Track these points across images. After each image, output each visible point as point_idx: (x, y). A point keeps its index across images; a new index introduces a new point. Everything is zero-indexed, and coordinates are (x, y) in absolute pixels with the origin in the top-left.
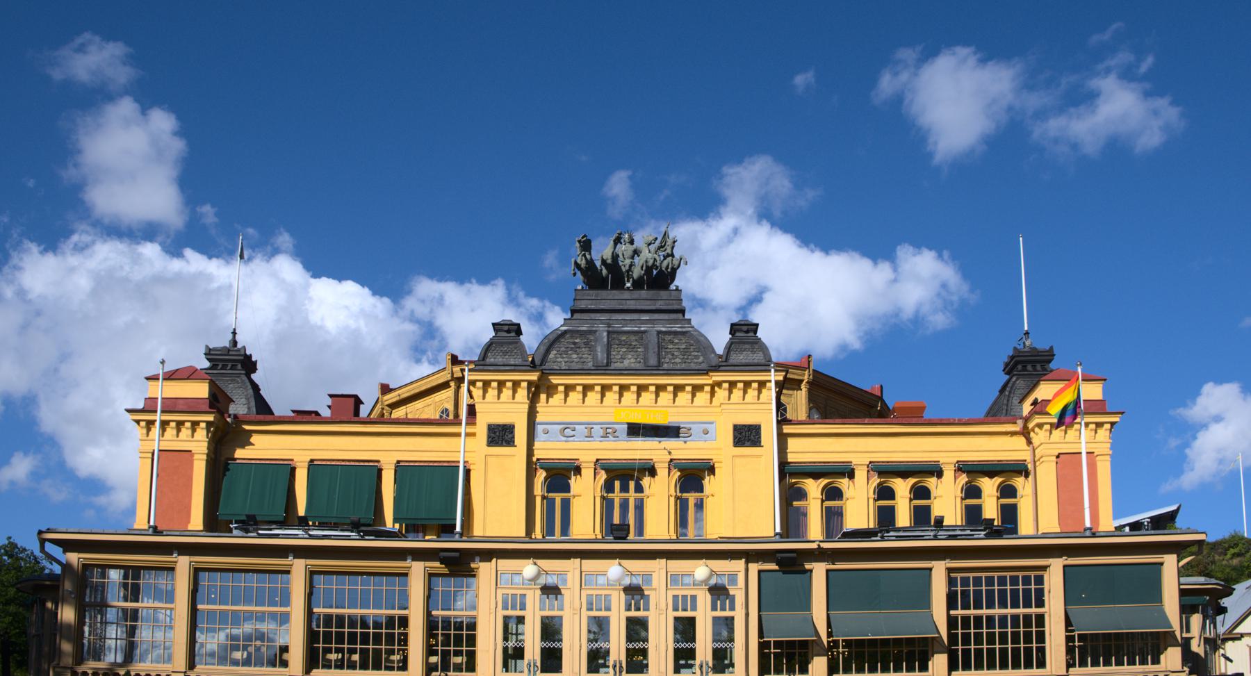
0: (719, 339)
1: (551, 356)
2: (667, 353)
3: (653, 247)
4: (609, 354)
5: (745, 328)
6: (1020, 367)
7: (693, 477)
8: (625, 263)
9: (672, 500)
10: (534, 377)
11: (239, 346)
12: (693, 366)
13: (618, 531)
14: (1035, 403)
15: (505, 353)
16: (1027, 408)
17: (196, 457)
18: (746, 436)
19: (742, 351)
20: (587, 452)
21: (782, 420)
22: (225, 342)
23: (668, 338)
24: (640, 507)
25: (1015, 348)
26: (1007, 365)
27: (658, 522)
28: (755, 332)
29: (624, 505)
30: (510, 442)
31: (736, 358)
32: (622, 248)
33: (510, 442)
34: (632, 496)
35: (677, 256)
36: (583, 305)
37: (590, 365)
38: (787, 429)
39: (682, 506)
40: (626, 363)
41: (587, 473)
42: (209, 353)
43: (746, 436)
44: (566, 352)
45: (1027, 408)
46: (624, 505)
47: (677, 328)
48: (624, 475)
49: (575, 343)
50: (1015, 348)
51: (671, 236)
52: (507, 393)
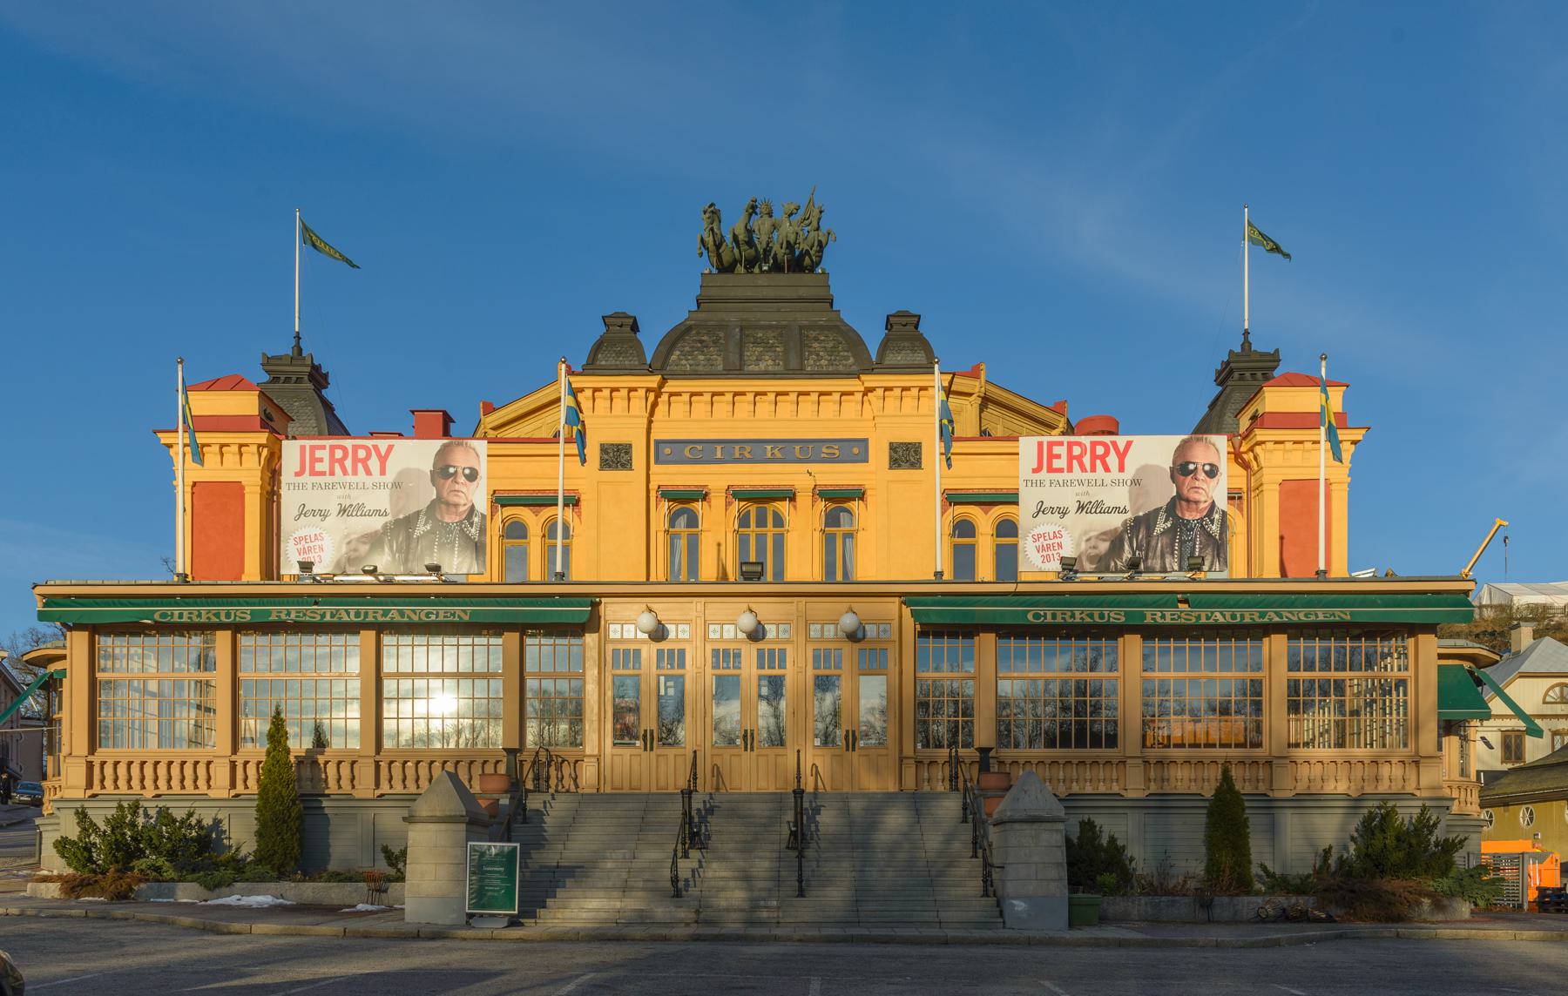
0: (873, 337)
1: (673, 357)
2: (811, 353)
3: (797, 218)
4: (741, 355)
5: (904, 320)
6: (1236, 375)
7: (838, 500)
8: (761, 241)
9: (817, 535)
10: (653, 381)
11: (304, 354)
12: (841, 368)
13: (751, 573)
14: (1254, 418)
15: (619, 354)
16: (1245, 422)
17: (247, 490)
18: (905, 456)
19: (900, 350)
20: (1233, 717)
21: (947, 435)
22: (285, 349)
23: (813, 334)
24: (779, 542)
25: (1231, 352)
26: (1219, 373)
27: (803, 559)
28: (916, 327)
29: (761, 539)
30: (626, 465)
31: (892, 359)
32: (756, 222)
33: (626, 465)
34: (770, 530)
35: (824, 229)
36: (713, 292)
37: (720, 368)
38: (957, 447)
39: (829, 541)
40: (762, 366)
41: (718, 500)
42: (268, 362)
43: (905, 456)
44: (691, 353)
45: (1245, 422)
46: (761, 539)
47: (823, 319)
48: (760, 502)
49: (701, 342)
50: (1231, 352)
51: (818, 203)
52: (620, 403)
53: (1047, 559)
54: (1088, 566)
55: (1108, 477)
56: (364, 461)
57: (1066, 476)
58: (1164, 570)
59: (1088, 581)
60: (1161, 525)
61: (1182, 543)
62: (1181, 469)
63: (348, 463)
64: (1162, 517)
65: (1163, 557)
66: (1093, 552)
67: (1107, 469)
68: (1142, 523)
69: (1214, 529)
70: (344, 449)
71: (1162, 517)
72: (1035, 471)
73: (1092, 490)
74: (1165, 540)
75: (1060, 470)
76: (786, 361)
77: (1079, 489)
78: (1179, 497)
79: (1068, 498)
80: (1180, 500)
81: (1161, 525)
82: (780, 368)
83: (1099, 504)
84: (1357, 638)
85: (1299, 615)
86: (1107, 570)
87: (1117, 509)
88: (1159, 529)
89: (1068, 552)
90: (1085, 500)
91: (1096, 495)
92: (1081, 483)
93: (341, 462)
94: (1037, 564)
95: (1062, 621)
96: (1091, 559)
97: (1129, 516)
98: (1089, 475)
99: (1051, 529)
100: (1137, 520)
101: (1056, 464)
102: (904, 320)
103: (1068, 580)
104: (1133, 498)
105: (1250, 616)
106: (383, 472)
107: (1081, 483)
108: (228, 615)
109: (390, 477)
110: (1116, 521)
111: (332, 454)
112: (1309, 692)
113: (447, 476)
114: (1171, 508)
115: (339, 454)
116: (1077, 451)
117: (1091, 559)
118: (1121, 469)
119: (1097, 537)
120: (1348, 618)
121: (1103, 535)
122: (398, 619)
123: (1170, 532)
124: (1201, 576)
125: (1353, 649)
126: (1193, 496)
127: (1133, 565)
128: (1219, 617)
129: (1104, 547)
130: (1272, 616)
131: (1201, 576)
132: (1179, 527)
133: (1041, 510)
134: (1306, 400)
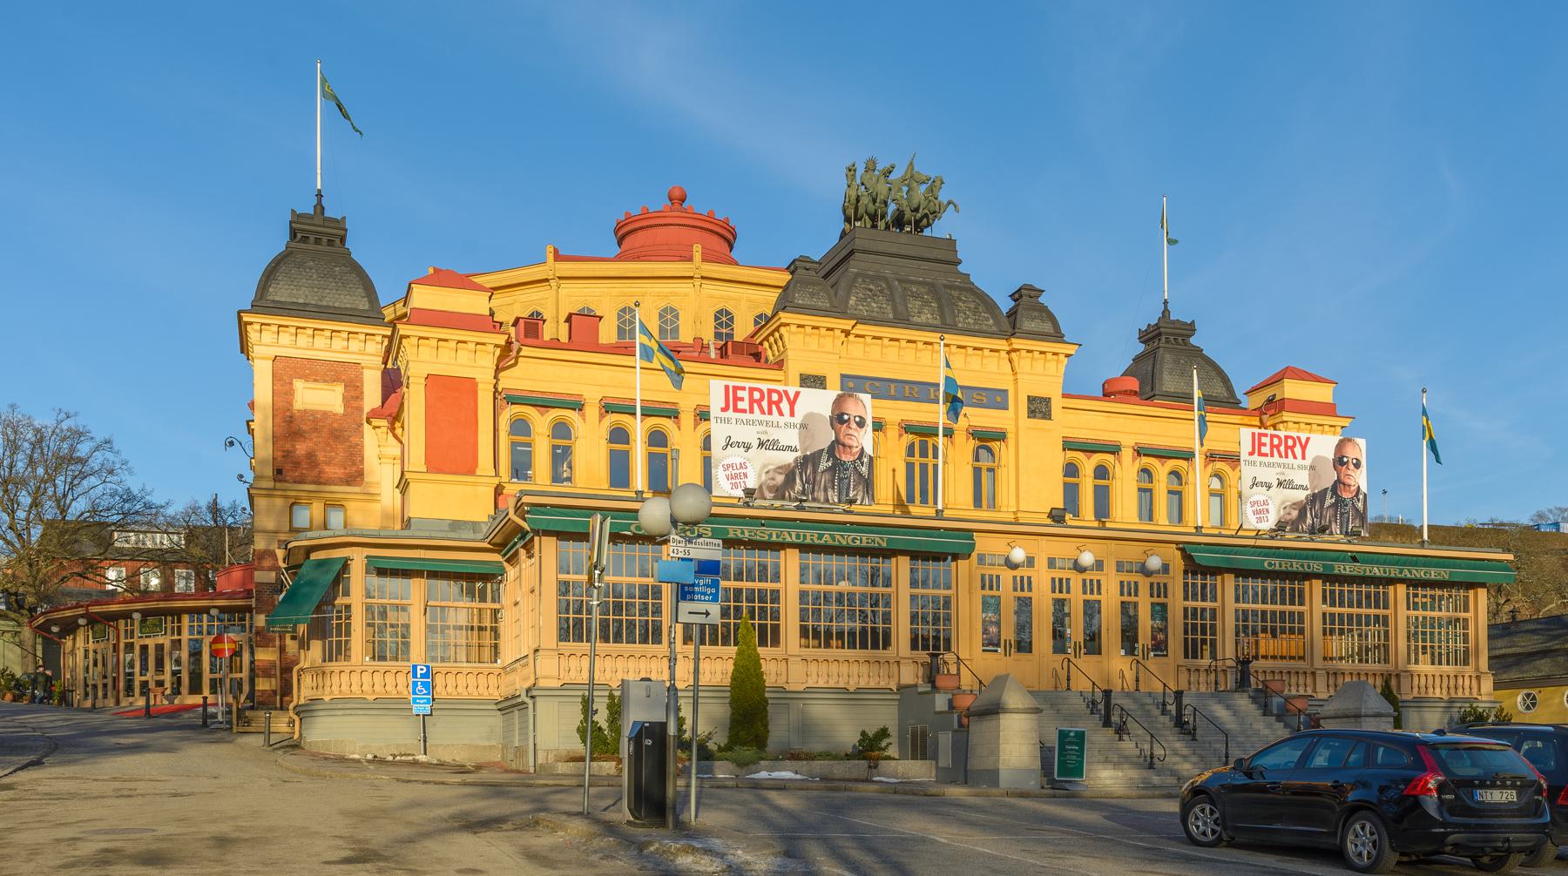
1: (851, 302)
15: (812, 295)
40: (923, 319)
53: (735, 486)
54: (769, 495)
55: (782, 420)
56: (777, 403)
57: (747, 416)
58: (827, 501)
59: (1289, 541)
60: (824, 464)
61: (840, 480)
62: (838, 419)
63: (1282, 448)
64: (825, 456)
65: (826, 490)
66: (772, 483)
67: (781, 414)
68: (809, 461)
69: (1360, 505)
70: (760, 391)
71: (1329, 494)
72: (724, 410)
73: (769, 430)
74: (827, 476)
75: (744, 411)
76: (943, 317)
77: (1279, 470)
78: (837, 442)
79: (1271, 476)
80: (1338, 484)
81: (824, 464)
82: (937, 322)
83: (776, 442)
84: (1359, 584)
85: (811, 537)
86: (783, 498)
87: (789, 448)
88: (1327, 503)
89: (752, 483)
90: (1282, 478)
91: (773, 434)
92: (761, 423)
93: (759, 402)
94: (725, 487)
95: (1272, 570)
96: (770, 489)
97: (799, 454)
98: (1283, 460)
99: (738, 461)
100: (805, 458)
101: (741, 405)
102: (808, 265)
103: (747, 505)
104: (802, 439)
105: (1296, 565)
106: (792, 414)
107: (761, 423)
108: (798, 537)
109: (798, 419)
110: (789, 458)
111: (751, 395)
112: (1350, 622)
113: (842, 422)
114: (831, 450)
115: (757, 395)
116: (757, 395)
117: (770, 489)
118: (792, 414)
119: (775, 470)
120: (884, 545)
121: (779, 469)
122: (831, 542)
123: (831, 470)
124: (854, 508)
125: (1341, 592)
126: (847, 441)
127: (1312, 531)
128: (827, 539)
129: (780, 479)
130: (1393, 572)
131: (854, 508)
132: (837, 466)
133: (729, 444)
134: (1321, 393)
